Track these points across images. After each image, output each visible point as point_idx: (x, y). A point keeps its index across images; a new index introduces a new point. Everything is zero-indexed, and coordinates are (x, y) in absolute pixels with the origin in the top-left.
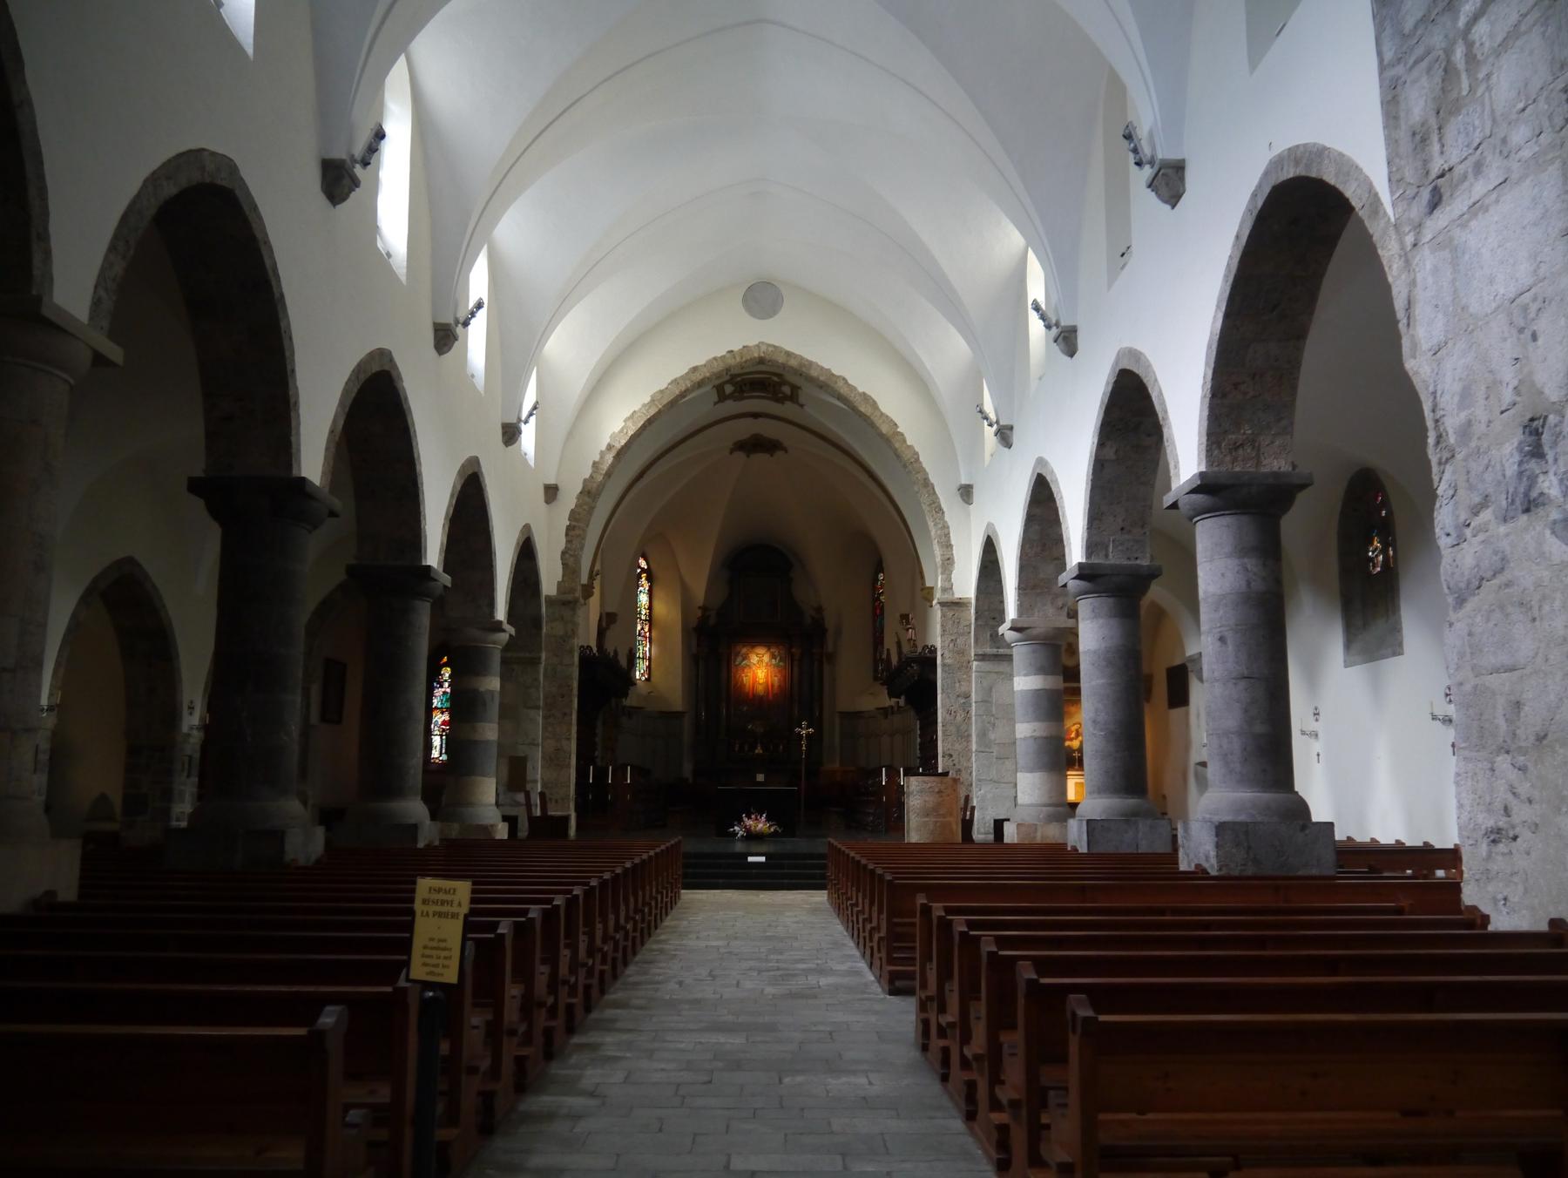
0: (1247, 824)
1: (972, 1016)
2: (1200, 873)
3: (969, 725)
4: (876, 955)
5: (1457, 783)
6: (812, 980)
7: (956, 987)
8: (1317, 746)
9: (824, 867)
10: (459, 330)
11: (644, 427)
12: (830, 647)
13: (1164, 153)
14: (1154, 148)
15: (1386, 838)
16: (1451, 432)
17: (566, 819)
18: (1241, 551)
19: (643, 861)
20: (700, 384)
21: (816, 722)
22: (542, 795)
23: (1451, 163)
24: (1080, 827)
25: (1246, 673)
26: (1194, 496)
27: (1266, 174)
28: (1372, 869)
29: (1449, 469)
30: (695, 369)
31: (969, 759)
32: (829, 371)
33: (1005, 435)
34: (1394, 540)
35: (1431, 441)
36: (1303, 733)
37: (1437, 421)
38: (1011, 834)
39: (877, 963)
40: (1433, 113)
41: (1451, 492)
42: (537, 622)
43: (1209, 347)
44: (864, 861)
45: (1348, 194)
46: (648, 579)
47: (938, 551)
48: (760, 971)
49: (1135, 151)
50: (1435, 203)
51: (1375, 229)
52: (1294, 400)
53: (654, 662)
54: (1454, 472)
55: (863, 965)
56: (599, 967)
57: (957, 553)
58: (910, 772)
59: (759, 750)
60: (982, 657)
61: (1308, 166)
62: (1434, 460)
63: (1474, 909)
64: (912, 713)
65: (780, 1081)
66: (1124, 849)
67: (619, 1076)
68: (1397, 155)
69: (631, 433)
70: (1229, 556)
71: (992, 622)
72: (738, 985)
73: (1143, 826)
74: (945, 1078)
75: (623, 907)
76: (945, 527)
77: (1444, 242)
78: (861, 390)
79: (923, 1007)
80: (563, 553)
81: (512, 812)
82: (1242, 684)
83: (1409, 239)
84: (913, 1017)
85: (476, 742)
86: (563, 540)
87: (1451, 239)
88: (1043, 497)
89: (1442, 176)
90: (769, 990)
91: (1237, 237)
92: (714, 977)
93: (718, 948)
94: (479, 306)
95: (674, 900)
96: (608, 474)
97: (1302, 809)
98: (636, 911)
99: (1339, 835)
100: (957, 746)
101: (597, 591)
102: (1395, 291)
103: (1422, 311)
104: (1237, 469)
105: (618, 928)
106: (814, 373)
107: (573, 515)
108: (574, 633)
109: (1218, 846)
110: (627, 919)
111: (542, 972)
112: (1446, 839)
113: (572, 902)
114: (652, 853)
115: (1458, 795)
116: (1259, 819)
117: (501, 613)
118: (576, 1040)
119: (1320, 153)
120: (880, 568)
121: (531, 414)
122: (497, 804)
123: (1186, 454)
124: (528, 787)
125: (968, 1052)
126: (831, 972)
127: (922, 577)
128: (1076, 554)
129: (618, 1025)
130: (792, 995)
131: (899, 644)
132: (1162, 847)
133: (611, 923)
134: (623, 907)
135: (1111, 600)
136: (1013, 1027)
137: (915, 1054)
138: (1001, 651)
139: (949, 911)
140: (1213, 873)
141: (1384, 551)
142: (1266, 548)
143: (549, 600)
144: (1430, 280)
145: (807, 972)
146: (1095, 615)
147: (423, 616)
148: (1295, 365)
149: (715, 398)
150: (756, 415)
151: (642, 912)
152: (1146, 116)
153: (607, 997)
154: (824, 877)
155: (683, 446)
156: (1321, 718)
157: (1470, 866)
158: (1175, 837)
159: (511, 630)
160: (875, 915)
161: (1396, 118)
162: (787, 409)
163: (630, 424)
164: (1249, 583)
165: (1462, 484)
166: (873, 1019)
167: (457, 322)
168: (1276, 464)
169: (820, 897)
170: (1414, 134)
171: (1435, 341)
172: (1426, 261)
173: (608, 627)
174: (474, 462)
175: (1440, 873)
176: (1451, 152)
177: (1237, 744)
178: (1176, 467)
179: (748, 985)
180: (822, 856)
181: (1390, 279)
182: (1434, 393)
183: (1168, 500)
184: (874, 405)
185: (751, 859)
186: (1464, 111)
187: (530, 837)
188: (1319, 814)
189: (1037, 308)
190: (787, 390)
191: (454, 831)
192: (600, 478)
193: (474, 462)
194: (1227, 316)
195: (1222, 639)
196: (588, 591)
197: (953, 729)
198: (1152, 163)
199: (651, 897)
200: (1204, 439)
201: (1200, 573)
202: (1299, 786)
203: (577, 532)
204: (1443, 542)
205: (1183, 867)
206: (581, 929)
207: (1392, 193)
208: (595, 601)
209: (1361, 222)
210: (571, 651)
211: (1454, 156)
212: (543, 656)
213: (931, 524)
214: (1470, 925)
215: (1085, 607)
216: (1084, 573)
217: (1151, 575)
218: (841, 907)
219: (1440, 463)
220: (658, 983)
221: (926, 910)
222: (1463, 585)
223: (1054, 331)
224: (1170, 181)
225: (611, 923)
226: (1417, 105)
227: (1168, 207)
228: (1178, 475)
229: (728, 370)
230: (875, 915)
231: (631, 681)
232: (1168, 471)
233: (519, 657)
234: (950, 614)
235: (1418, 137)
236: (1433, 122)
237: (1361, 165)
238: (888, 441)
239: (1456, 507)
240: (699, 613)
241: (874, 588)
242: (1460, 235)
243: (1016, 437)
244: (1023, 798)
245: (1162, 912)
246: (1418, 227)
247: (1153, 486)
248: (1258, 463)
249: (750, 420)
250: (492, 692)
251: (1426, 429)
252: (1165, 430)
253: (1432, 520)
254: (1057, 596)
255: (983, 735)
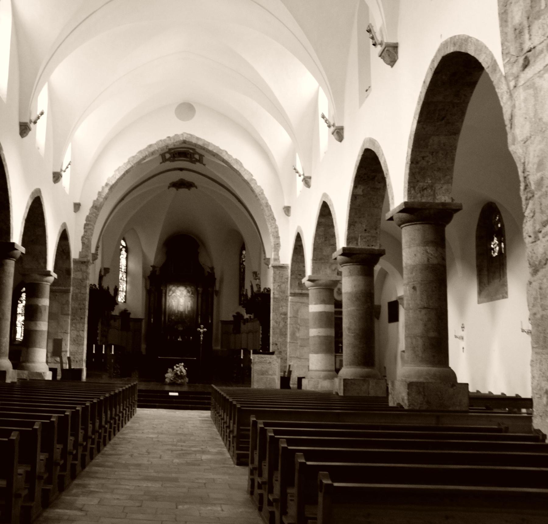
0: (424, 383)
1: (274, 479)
2: (399, 407)
3: (286, 329)
4: (231, 445)
5: (531, 365)
6: (198, 456)
7: (267, 464)
8: (462, 344)
9: (209, 399)
10: (32, 125)
11: (124, 175)
12: (217, 287)
13: (388, 39)
14: (382, 37)
15: (497, 391)
16: (532, 183)
17: (80, 371)
18: (426, 243)
19: (116, 394)
20: (153, 153)
21: (209, 326)
22: (69, 358)
23: (535, 45)
24: (340, 383)
25: (426, 305)
26: (401, 214)
27: (439, 50)
28: (488, 408)
29: (531, 202)
30: (150, 146)
31: (286, 347)
32: (217, 147)
33: (307, 181)
34: (504, 239)
35: (522, 188)
36: (456, 337)
37: (525, 178)
38: (306, 385)
39: (232, 449)
40: (526, 19)
41: (532, 215)
42: (68, 272)
43: (410, 138)
44: (228, 397)
45: (481, 60)
46: (127, 251)
47: (272, 240)
48: (172, 451)
49: (373, 38)
50: (526, 64)
51: (494, 78)
52: (453, 166)
53: (127, 292)
54: (534, 204)
55: (225, 450)
56: (89, 446)
57: (282, 241)
58: (255, 352)
59: (179, 339)
60: (294, 295)
61: (460, 46)
62: (523, 198)
63: (539, 431)
64: (258, 322)
65: (177, 508)
66: (362, 394)
67: (96, 501)
68: (507, 41)
69: (117, 177)
70: (418, 245)
71: (299, 277)
72: (160, 458)
73: (372, 383)
74: (260, 509)
75: (104, 416)
76: (276, 227)
77: (531, 85)
78: (234, 157)
79: (252, 473)
80: (83, 237)
81: (54, 366)
82: (423, 312)
83: (512, 84)
84: (247, 477)
85: (36, 331)
86: (83, 231)
87: (534, 84)
88: (325, 212)
89: (530, 51)
90: (176, 461)
91: (424, 82)
92: (149, 453)
93: (152, 438)
94: (42, 114)
95: (131, 414)
96: (106, 198)
97: (453, 376)
98: (111, 418)
99: (471, 389)
100: (280, 340)
101: (99, 257)
102: (504, 110)
103: (518, 121)
104: (424, 201)
105: (101, 426)
106: (210, 148)
107: (88, 219)
108: (87, 278)
109: (409, 394)
110: (106, 422)
111: (58, 448)
112: (526, 394)
113: (75, 414)
114: (127, 387)
115: (532, 371)
116: (430, 381)
117: (50, 266)
118: (76, 482)
119: (466, 39)
120: (243, 248)
121: (67, 168)
122: (47, 362)
123: (398, 193)
124: (63, 354)
125: (271, 498)
126: (208, 453)
127: (265, 253)
128: (341, 242)
129: (98, 475)
130: (188, 464)
131: (252, 287)
132: (380, 394)
133: (97, 424)
134: (104, 416)
135: (359, 267)
136: (292, 485)
137: (248, 496)
138: (304, 292)
139: (266, 424)
140: (406, 408)
141: (499, 245)
142: (438, 241)
143: (75, 261)
144: (523, 105)
145: (195, 452)
146: (351, 274)
147: (11, 266)
148: (453, 148)
149: (161, 161)
150: (181, 169)
151: (115, 419)
152: (378, 22)
153: (94, 461)
154: (209, 404)
155: (146, 183)
156: (465, 329)
157: (537, 408)
158: (387, 388)
159: (55, 275)
160: (231, 425)
161: (506, 21)
162: (197, 167)
163: (117, 173)
164: (428, 260)
165: (538, 210)
166: (227, 477)
167: (31, 121)
168: (443, 198)
169: (207, 414)
170: (515, 30)
171: (525, 136)
172: (521, 94)
173: (105, 275)
174: (38, 191)
175: (524, 410)
176: (535, 38)
177: (420, 342)
178: (392, 199)
179: (166, 457)
180: (209, 394)
181: (502, 104)
182: (524, 163)
183: (388, 216)
184: (241, 165)
185: (171, 394)
186: (542, 17)
187: (61, 379)
188: (461, 379)
189: (323, 117)
190: (197, 157)
191: (25, 375)
192: (101, 200)
193: (38, 191)
194: (419, 122)
195: (414, 288)
196: (95, 257)
197: (278, 331)
198: (381, 44)
199: (120, 412)
200: (407, 185)
201: (404, 254)
202: (452, 364)
203: (90, 227)
204: (528, 240)
205: (391, 404)
206: (80, 426)
207: (504, 60)
208: (98, 262)
209: (487, 74)
210: (85, 287)
211: (536, 40)
212: (71, 289)
213: (269, 226)
214: (536, 439)
215: (345, 270)
216: (346, 252)
217: (381, 253)
218: (216, 419)
219: (526, 199)
220: (121, 455)
221: (255, 423)
222: (537, 263)
223: (332, 129)
224: (390, 53)
225: (97, 424)
226: (517, 15)
227: (389, 67)
228: (393, 203)
229: (167, 146)
230: (231, 425)
231: (116, 303)
232: (388, 201)
233: (59, 290)
234: (278, 272)
235: (517, 31)
236: (526, 23)
237: (488, 46)
238: (246, 184)
239: (534, 223)
240: (151, 269)
241: (240, 258)
242: (539, 82)
243: (313, 182)
244: (312, 367)
245: (377, 428)
246: (517, 77)
247: (381, 209)
248: (435, 198)
249: (179, 172)
250: (45, 306)
251: (519, 182)
252: (387, 180)
253: (522, 228)
254: (332, 264)
255: (293, 334)
